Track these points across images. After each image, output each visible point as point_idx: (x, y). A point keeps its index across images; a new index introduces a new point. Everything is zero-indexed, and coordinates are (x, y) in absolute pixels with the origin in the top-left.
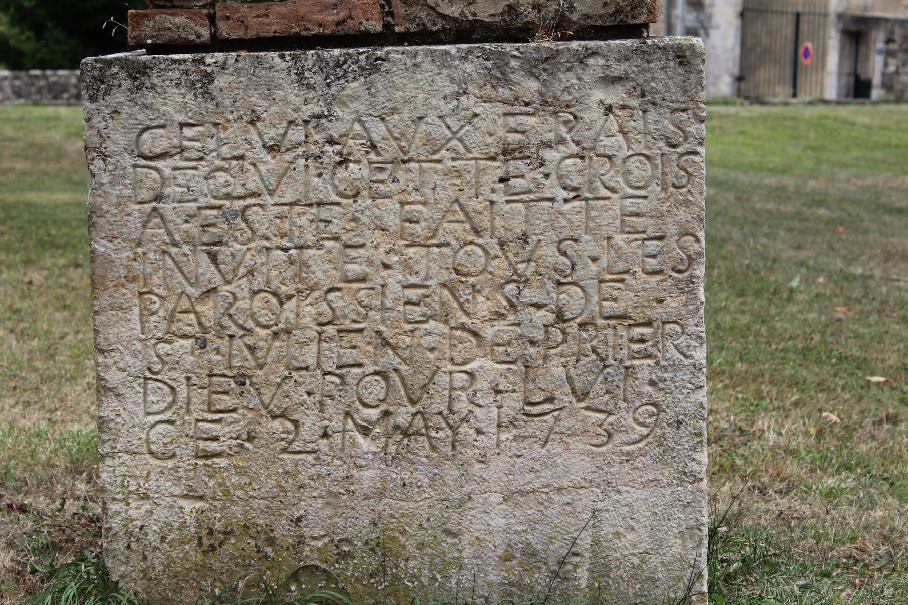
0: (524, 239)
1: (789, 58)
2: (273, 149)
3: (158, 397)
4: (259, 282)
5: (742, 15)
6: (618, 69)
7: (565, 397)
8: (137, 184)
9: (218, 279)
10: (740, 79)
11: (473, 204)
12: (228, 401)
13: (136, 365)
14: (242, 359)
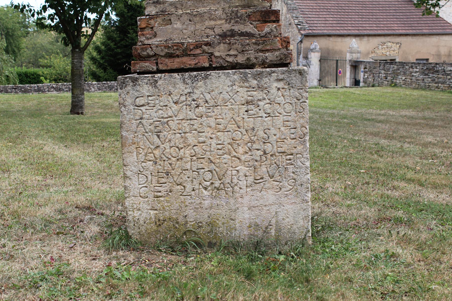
0: (253, 129)
1: (335, 74)
2: (176, 103)
3: (142, 179)
4: (172, 144)
5: (320, 61)
6: (281, 77)
7: (266, 177)
8: (135, 114)
9: (160, 143)
10: (320, 80)
11: (237, 119)
12: (163, 180)
13: (135, 170)
14: (167, 167)
